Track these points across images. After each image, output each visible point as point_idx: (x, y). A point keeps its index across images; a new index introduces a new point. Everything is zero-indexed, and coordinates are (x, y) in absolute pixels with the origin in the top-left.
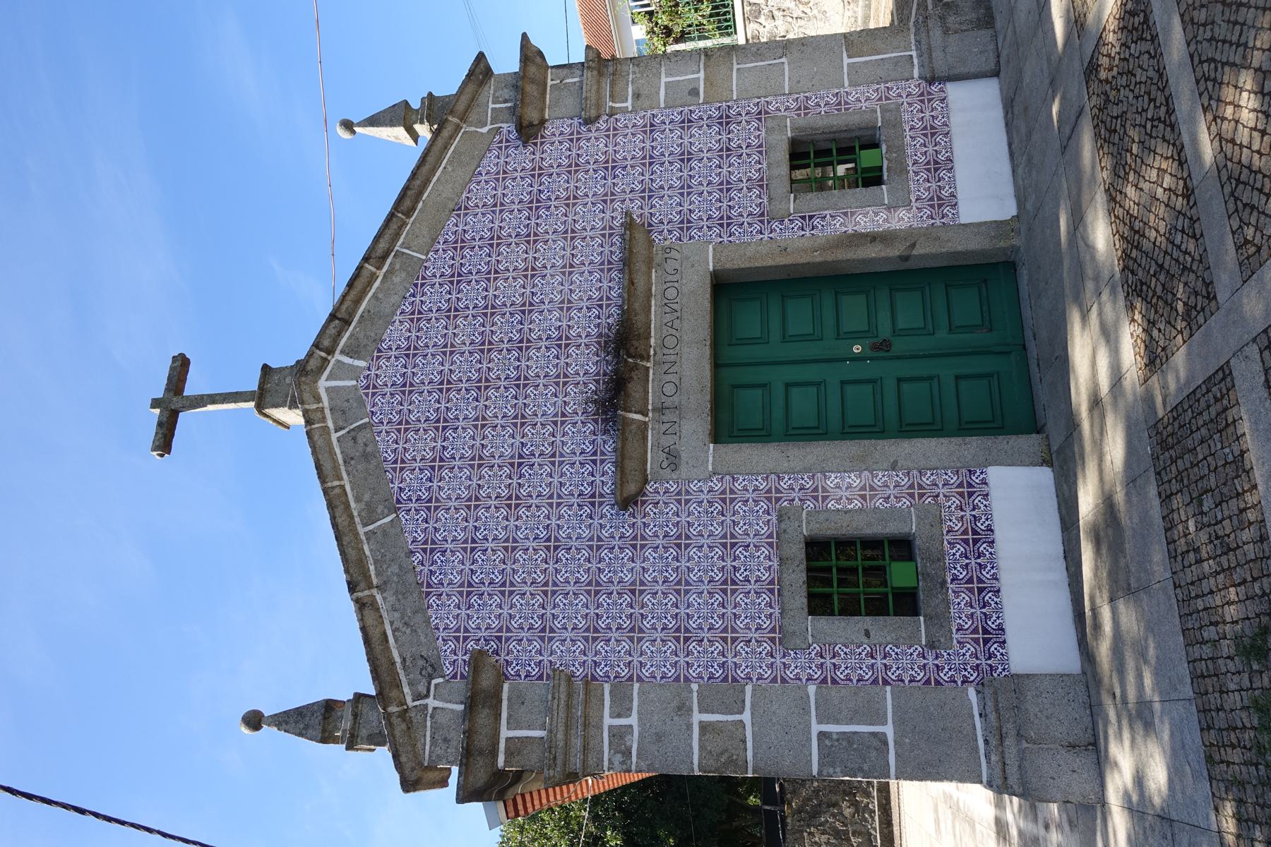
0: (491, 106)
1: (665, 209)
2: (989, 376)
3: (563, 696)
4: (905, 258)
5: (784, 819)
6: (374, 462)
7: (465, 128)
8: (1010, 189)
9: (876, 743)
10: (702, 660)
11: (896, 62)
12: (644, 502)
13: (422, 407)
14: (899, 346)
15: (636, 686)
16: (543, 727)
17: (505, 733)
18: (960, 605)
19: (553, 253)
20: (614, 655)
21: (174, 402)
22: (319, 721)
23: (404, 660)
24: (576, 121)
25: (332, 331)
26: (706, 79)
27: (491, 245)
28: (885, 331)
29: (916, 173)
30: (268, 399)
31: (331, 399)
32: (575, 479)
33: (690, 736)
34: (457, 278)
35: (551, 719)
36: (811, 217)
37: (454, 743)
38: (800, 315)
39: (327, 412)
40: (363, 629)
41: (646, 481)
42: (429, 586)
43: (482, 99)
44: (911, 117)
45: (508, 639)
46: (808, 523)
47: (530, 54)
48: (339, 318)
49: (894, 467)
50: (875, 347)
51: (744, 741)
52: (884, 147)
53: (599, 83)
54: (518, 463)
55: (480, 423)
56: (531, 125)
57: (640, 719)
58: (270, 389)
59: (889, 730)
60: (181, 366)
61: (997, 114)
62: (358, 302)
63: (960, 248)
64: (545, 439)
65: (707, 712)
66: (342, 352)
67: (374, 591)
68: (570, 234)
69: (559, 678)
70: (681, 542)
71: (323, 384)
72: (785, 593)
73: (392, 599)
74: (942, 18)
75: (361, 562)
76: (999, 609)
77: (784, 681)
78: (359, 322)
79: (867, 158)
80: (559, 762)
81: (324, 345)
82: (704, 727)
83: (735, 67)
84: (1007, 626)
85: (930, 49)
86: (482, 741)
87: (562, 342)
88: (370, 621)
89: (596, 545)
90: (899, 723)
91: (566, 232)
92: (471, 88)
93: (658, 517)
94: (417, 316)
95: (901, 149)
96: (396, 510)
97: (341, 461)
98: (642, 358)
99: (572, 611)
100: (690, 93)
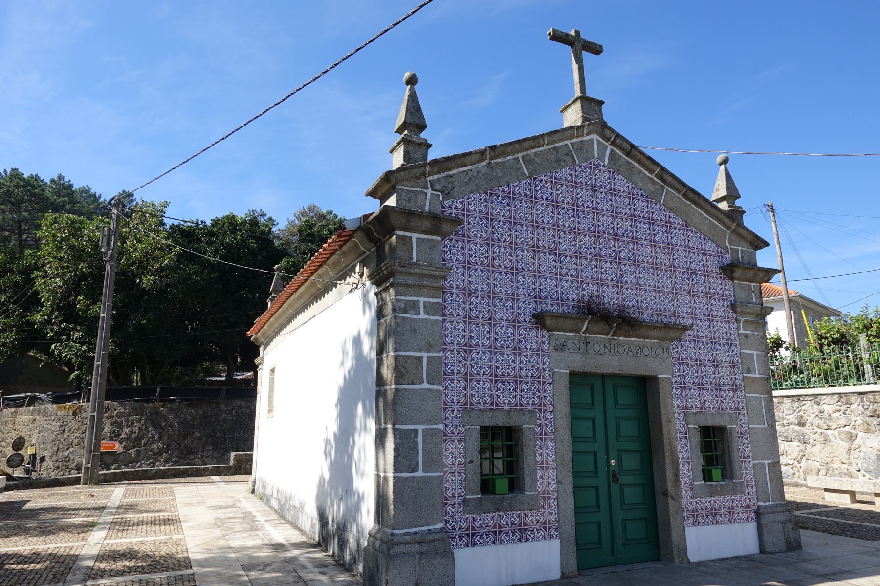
0: (740, 248)
1: (688, 349)
2: (600, 543)
3: (437, 273)
4: (665, 493)
5: (147, 401)
6: (556, 166)
7: (728, 232)
8: (703, 558)
9: (413, 465)
10: (455, 359)
11: (766, 492)
12: (537, 328)
13: (585, 197)
14: (615, 488)
15: (441, 319)
16: (418, 259)
17: (415, 236)
18: (486, 520)
19: (665, 281)
20: (457, 306)
21: (582, 46)
22: (415, 122)
23: (451, 176)
24: (733, 299)
25: (625, 145)
26: (755, 378)
27: (515, 223)
28: (624, 480)
29: (710, 502)
30: (586, 103)
31: (587, 141)
32: (549, 287)
33: (414, 351)
34: (651, 222)
35: (425, 266)
36: (686, 437)
37: (408, 204)
38: (629, 428)
39: (581, 139)
40: (471, 153)
41: (548, 330)
42: (491, 194)
43: (743, 243)
44: (738, 500)
45: (464, 241)
46: (529, 428)
47: (769, 273)
48: (631, 150)
49: (559, 482)
50: (614, 472)
51: (412, 384)
52: (722, 483)
53: (753, 314)
54: (556, 253)
55: (577, 231)
56: (733, 272)
57: (423, 320)
58: (591, 105)
59: (420, 473)
60: (596, 50)
61: (741, 553)
62: (639, 162)
63: (672, 526)
64: (569, 270)
65: (428, 361)
66: (612, 150)
67: (487, 161)
68: (675, 292)
69: (445, 272)
70: (517, 350)
71: (595, 137)
72: (492, 413)
73: (483, 171)
74: (790, 521)
75: (505, 154)
76: (485, 543)
77: (445, 409)
78: (628, 162)
79: (502, 484)
80: (402, 269)
81: (617, 140)
82: (420, 359)
83: (762, 396)
84: (476, 549)
85: (774, 513)
86: (415, 222)
87: (620, 284)
88: (475, 158)
89: (514, 297)
90: (424, 480)
91: (512, 273)
92: (750, 237)
93: (531, 337)
94: (631, 196)
95: (722, 494)
96: (530, 177)
97: (556, 145)
98: (614, 332)
99: (479, 282)
100: (748, 368)
